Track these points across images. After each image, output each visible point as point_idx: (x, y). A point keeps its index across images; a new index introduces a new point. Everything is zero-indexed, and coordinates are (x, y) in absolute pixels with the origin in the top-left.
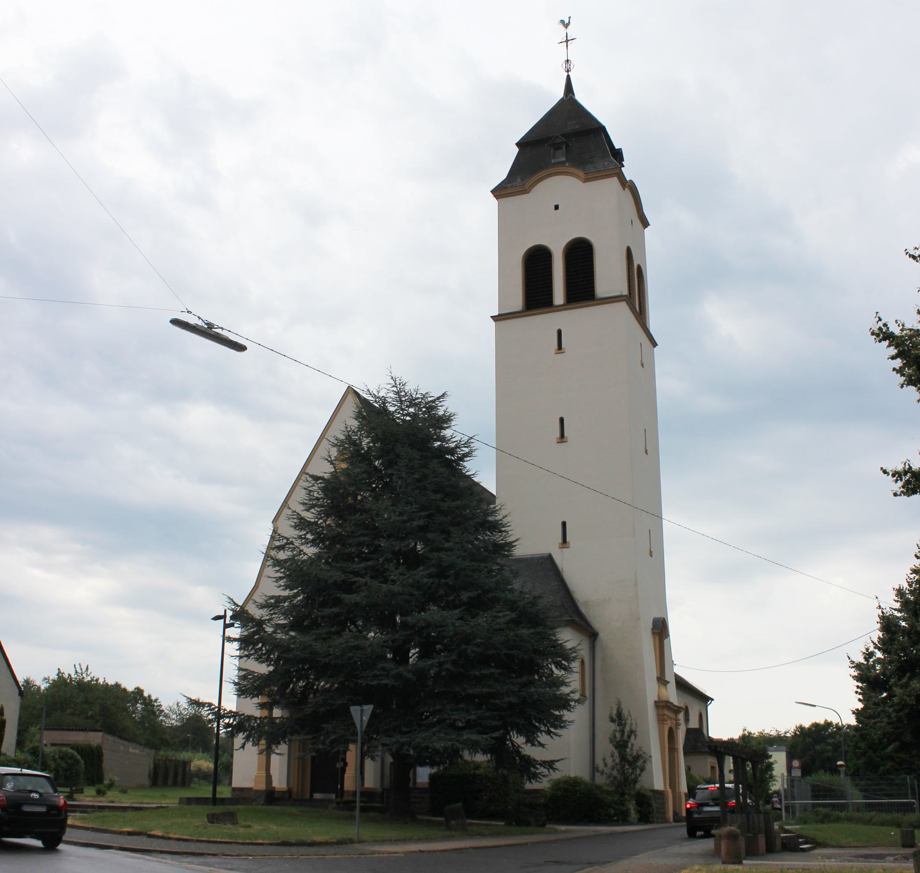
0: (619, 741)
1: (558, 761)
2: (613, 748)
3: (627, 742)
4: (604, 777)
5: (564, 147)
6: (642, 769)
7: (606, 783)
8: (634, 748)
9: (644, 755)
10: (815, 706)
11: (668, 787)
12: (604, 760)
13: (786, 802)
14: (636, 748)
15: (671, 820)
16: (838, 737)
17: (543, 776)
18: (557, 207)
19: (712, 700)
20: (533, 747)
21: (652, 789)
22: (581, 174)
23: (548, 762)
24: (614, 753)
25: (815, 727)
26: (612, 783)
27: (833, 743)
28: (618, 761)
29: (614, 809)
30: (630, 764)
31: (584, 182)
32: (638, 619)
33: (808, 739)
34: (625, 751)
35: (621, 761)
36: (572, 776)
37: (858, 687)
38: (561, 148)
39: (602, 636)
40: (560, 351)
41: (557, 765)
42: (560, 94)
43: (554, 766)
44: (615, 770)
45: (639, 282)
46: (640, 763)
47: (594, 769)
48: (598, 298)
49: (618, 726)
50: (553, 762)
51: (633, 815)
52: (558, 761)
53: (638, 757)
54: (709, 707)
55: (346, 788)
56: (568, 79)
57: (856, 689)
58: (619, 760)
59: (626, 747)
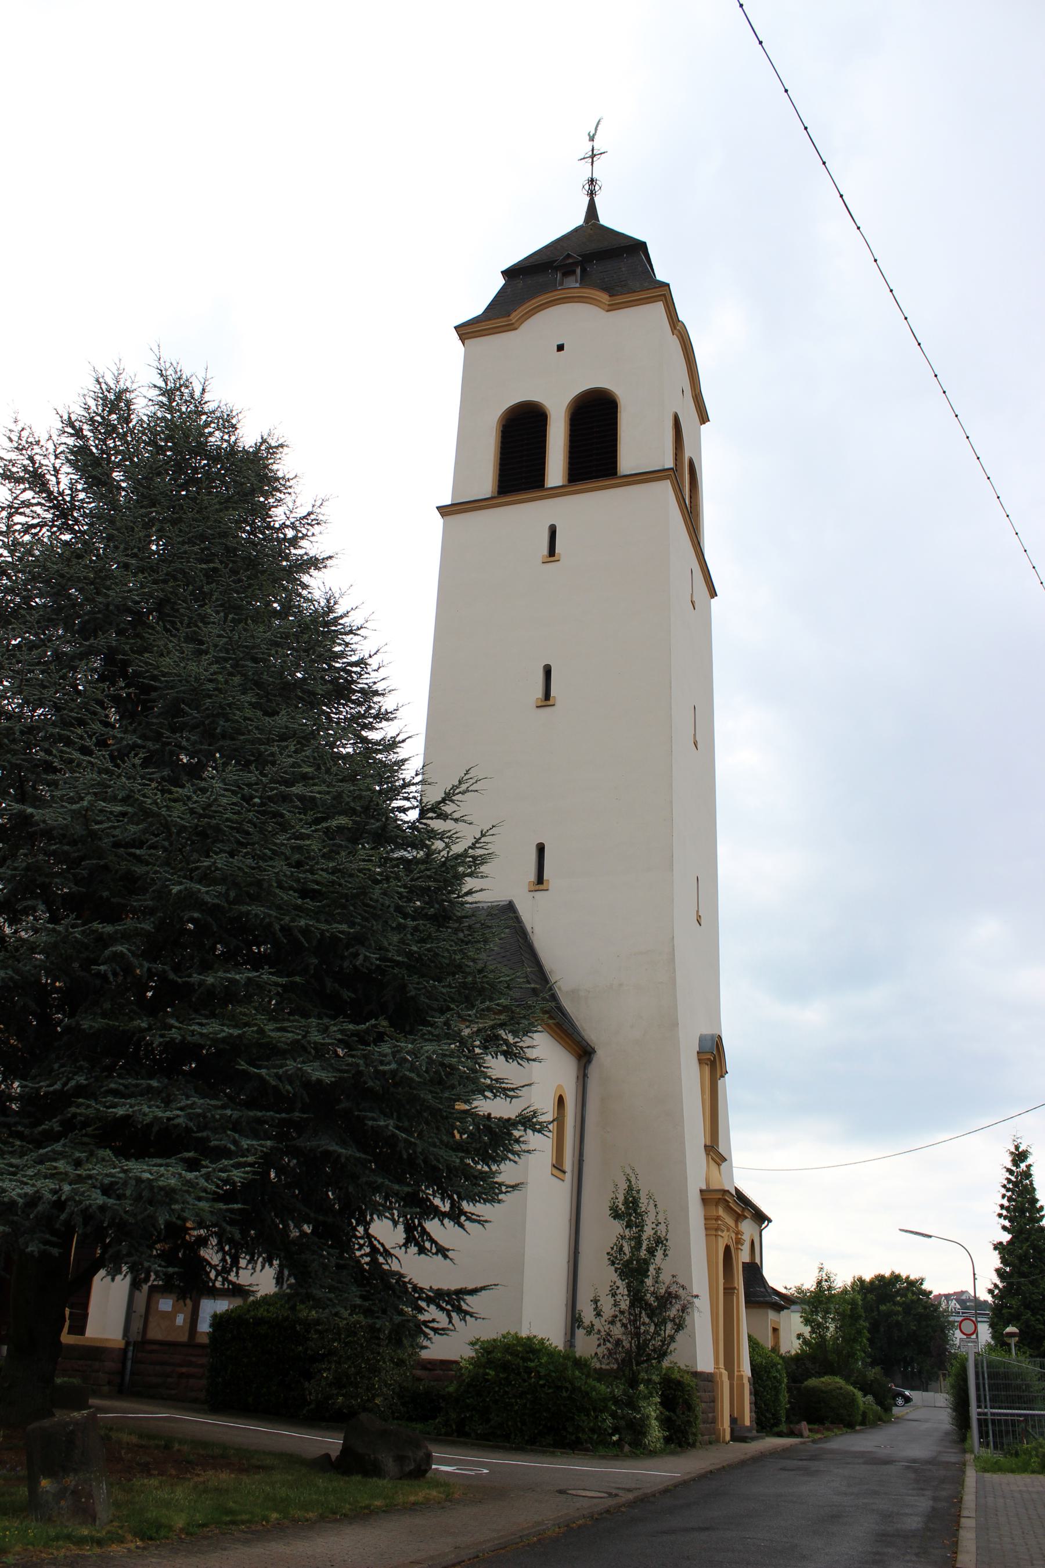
0: (629, 1262)
1: (473, 1292)
2: (615, 1277)
3: (646, 1262)
4: (594, 1339)
5: (578, 271)
6: (679, 1327)
7: (596, 1354)
8: (662, 1277)
9: (681, 1292)
10: (930, 1236)
11: (722, 1365)
12: (596, 1301)
13: (980, 1410)
14: (665, 1277)
15: (728, 1437)
16: (910, 1295)
17: (435, 1330)
18: (560, 348)
19: (770, 1221)
20: (423, 1256)
21: (694, 1370)
22: (604, 297)
23: (449, 1293)
24: (618, 1287)
25: (880, 1281)
26: (610, 1354)
27: (904, 1303)
28: (624, 1305)
29: (614, 1415)
30: (652, 1313)
31: (607, 311)
32: (675, 1025)
33: (870, 1296)
34: (643, 1282)
35: (632, 1305)
36: (524, 1334)
37: (1002, 1206)
38: (574, 272)
39: (602, 1056)
40: (552, 559)
41: (471, 1303)
43: (465, 1307)
44: (619, 1325)
45: (691, 483)
46: (673, 1312)
47: (574, 1320)
48: (622, 474)
49: (627, 1227)
50: (461, 1292)
51: (656, 1432)
52: (473, 1292)
53: (667, 1299)
54: (763, 1232)
57: (998, 1210)
58: (628, 1302)
59: (645, 1273)
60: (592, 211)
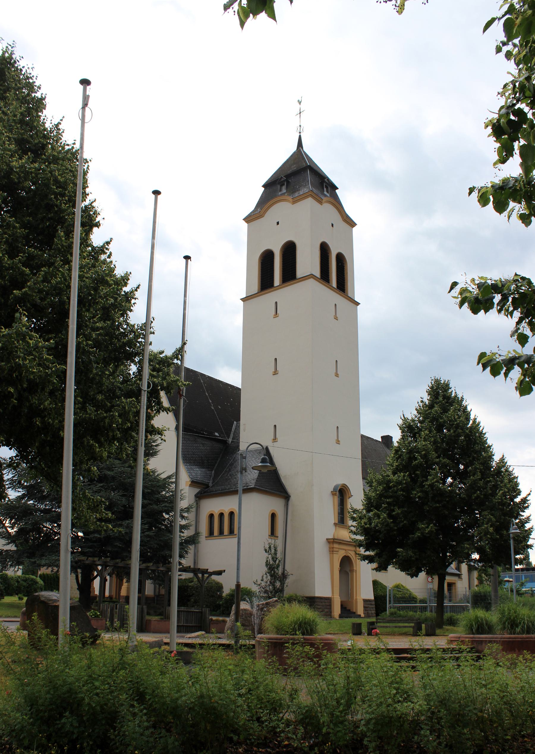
18: (278, 223)
42: (294, 148)
55: (122, 594)
56: (300, 137)
60: (300, 144)
